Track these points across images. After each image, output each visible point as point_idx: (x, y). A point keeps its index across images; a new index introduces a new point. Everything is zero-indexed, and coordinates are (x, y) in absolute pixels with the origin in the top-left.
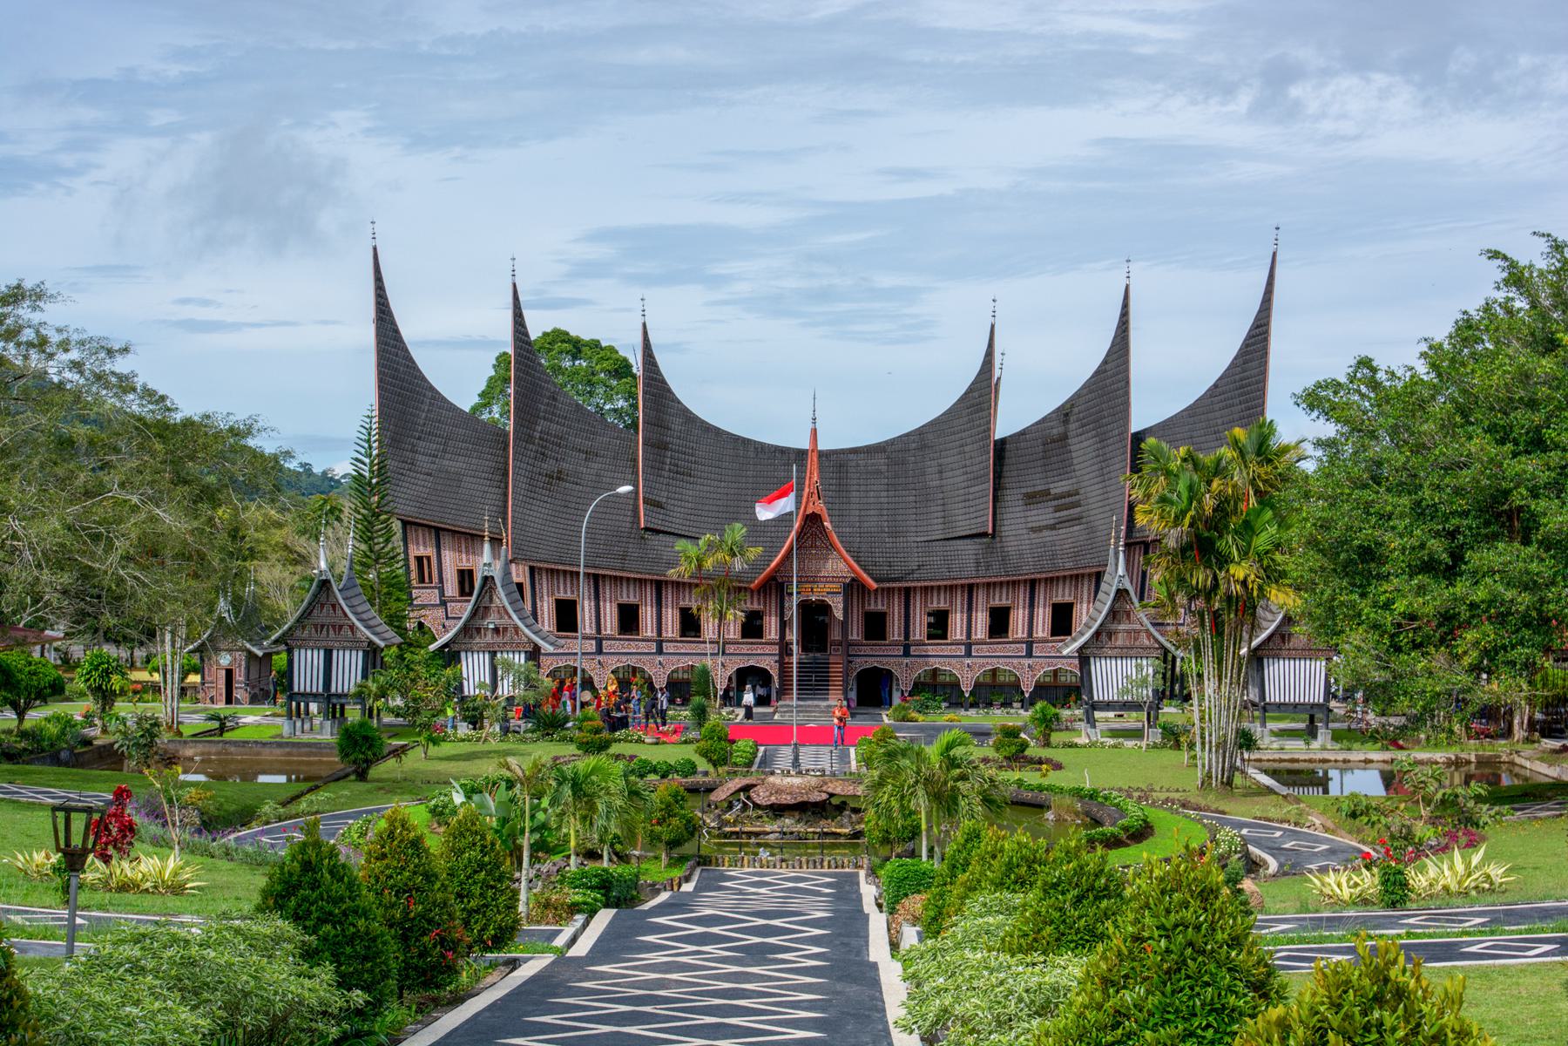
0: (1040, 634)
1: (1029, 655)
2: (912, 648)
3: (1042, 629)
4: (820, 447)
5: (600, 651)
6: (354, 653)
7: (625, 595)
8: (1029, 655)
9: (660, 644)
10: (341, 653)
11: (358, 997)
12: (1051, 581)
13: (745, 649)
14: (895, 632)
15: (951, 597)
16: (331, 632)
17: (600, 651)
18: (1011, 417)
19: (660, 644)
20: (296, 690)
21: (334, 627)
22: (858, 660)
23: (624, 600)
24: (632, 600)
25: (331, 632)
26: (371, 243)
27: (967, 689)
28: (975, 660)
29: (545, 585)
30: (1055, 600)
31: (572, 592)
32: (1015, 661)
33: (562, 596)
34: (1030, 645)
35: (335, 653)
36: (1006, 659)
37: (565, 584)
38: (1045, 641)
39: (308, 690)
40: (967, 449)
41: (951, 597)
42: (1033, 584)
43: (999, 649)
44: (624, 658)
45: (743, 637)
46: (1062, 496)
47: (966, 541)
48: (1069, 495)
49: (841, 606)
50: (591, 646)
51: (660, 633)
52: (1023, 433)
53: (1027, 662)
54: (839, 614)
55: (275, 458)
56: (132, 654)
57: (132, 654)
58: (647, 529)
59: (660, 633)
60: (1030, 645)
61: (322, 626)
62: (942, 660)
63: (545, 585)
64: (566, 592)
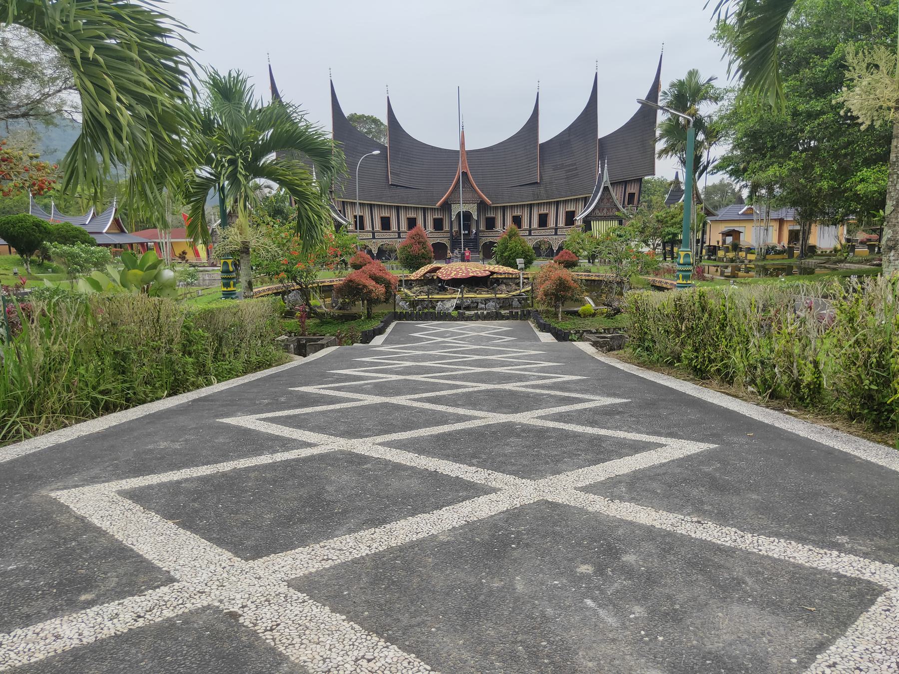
0: (561, 225)
1: (556, 234)
3: (561, 223)
4: (468, 148)
5: (374, 238)
8: (556, 234)
9: (399, 234)
11: (800, 378)
12: (566, 202)
13: (436, 235)
14: (551, 223)
17: (374, 238)
18: (547, 133)
19: (399, 234)
22: (484, 238)
23: (383, 215)
24: (387, 215)
26: (268, 63)
30: (382, 215)
32: (550, 237)
34: (556, 230)
38: (535, 230)
40: (528, 147)
42: (531, 206)
43: (543, 232)
44: (384, 240)
45: (539, 227)
46: (569, 166)
47: (528, 186)
48: (572, 165)
49: (476, 213)
50: (370, 235)
51: (399, 229)
52: (551, 140)
53: (554, 237)
54: (475, 217)
58: (392, 185)
59: (399, 229)
60: (556, 230)
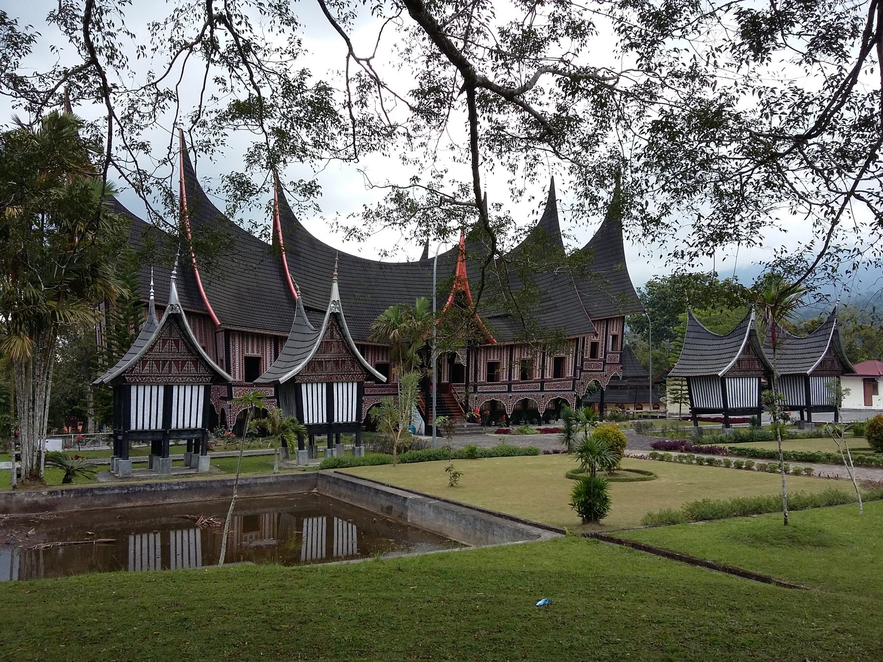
1: (542, 390)
2: (479, 387)
6: (320, 386)
7: (255, 351)
8: (542, 390)
10: (309, 386)
15: (501, 353)
16: (174, 368)
20: (133, 427)
21: (177, 362)
25: (174, 368)
27: (542, 412)
28: (514, 394)
29: (237, 345)
31: (258, 352)
32: (535, 394)
33: (250, 354)
35: (335, 386)
36: (527, 392)
37: (253, 345)
38: (550, 381)
39: (146, 427)
41: (501, 353)
42: (511, 348)
43: (527, 387)
53: (541, 394)
55: (22, 77)
56: (276, 176)
57: (276, 176)
60: (542, 383)
61: (165, 362)
62: (496, 395)
63: (237, 345)
64: (253, 352)
